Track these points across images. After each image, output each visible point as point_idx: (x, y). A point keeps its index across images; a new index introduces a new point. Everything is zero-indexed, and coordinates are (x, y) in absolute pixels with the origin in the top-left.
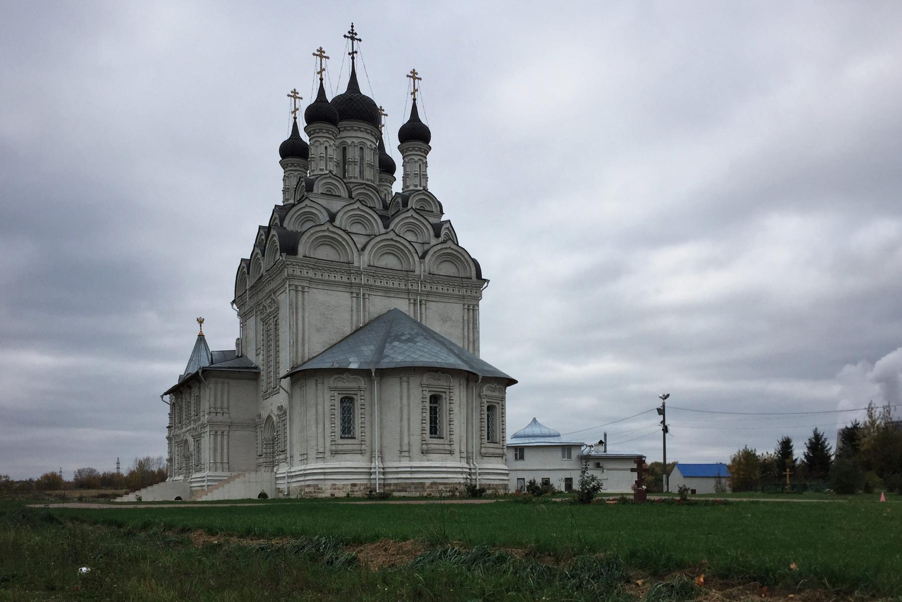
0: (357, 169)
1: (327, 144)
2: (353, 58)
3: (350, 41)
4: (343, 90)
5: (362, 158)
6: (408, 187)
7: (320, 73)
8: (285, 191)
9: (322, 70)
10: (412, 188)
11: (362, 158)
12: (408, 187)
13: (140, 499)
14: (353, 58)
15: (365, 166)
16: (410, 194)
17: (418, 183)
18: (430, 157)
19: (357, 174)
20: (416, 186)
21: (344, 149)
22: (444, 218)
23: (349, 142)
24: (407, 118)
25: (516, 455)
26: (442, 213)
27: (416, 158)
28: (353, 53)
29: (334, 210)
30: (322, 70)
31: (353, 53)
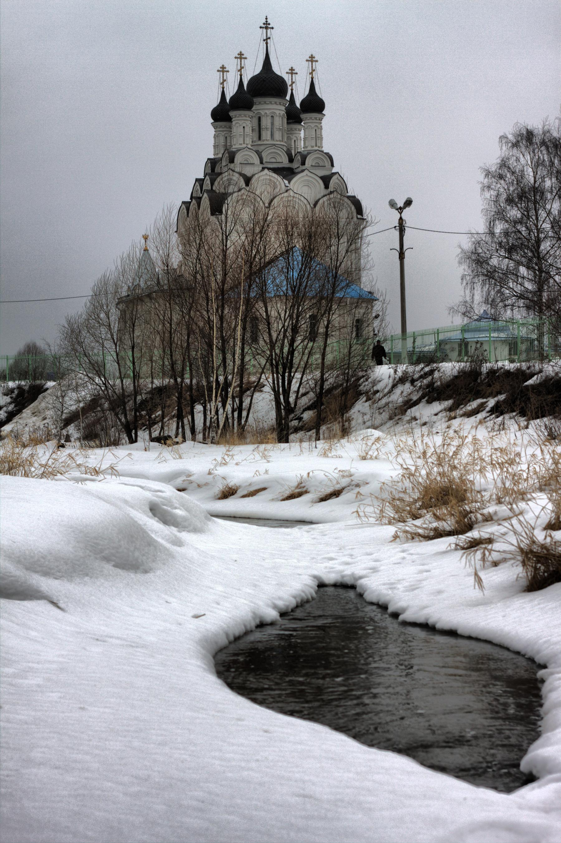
0: (269, 133)
1: (244, 125)
2: (267, 43)
3: (265, 30)
4: (258, 69)
5: (272, 124)
6: (306, 147)
7: (240, 70)
8: (215, 147)
9: (242, 68)
10: (309, 148)
11: (272, 124)
12: (306, 147)
13: (295, 392)
14: (267, 43)
15: (275, 130)
16: (309, 154)
17: (314, 144)
18: (324, 122)
19: (269, 137)
20: (312, 147)
21: (259, 119)
22: (334, 170)
23: (263, 113)
24: (307, 92)
25: (510, 351)
26: (332, 165)
27: (313, 125)
28: (267, 39)
29: (249, 175)
30: (242, 68)
31: (266, 40)
